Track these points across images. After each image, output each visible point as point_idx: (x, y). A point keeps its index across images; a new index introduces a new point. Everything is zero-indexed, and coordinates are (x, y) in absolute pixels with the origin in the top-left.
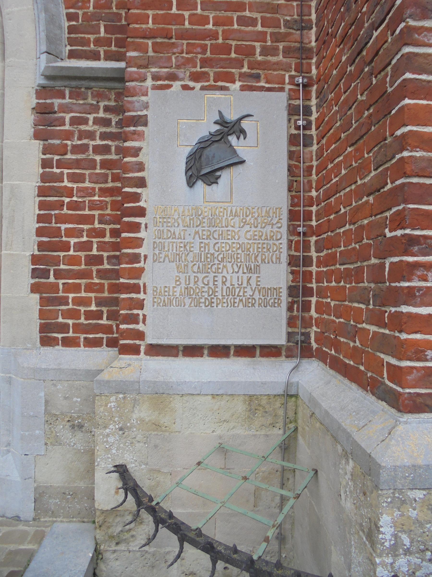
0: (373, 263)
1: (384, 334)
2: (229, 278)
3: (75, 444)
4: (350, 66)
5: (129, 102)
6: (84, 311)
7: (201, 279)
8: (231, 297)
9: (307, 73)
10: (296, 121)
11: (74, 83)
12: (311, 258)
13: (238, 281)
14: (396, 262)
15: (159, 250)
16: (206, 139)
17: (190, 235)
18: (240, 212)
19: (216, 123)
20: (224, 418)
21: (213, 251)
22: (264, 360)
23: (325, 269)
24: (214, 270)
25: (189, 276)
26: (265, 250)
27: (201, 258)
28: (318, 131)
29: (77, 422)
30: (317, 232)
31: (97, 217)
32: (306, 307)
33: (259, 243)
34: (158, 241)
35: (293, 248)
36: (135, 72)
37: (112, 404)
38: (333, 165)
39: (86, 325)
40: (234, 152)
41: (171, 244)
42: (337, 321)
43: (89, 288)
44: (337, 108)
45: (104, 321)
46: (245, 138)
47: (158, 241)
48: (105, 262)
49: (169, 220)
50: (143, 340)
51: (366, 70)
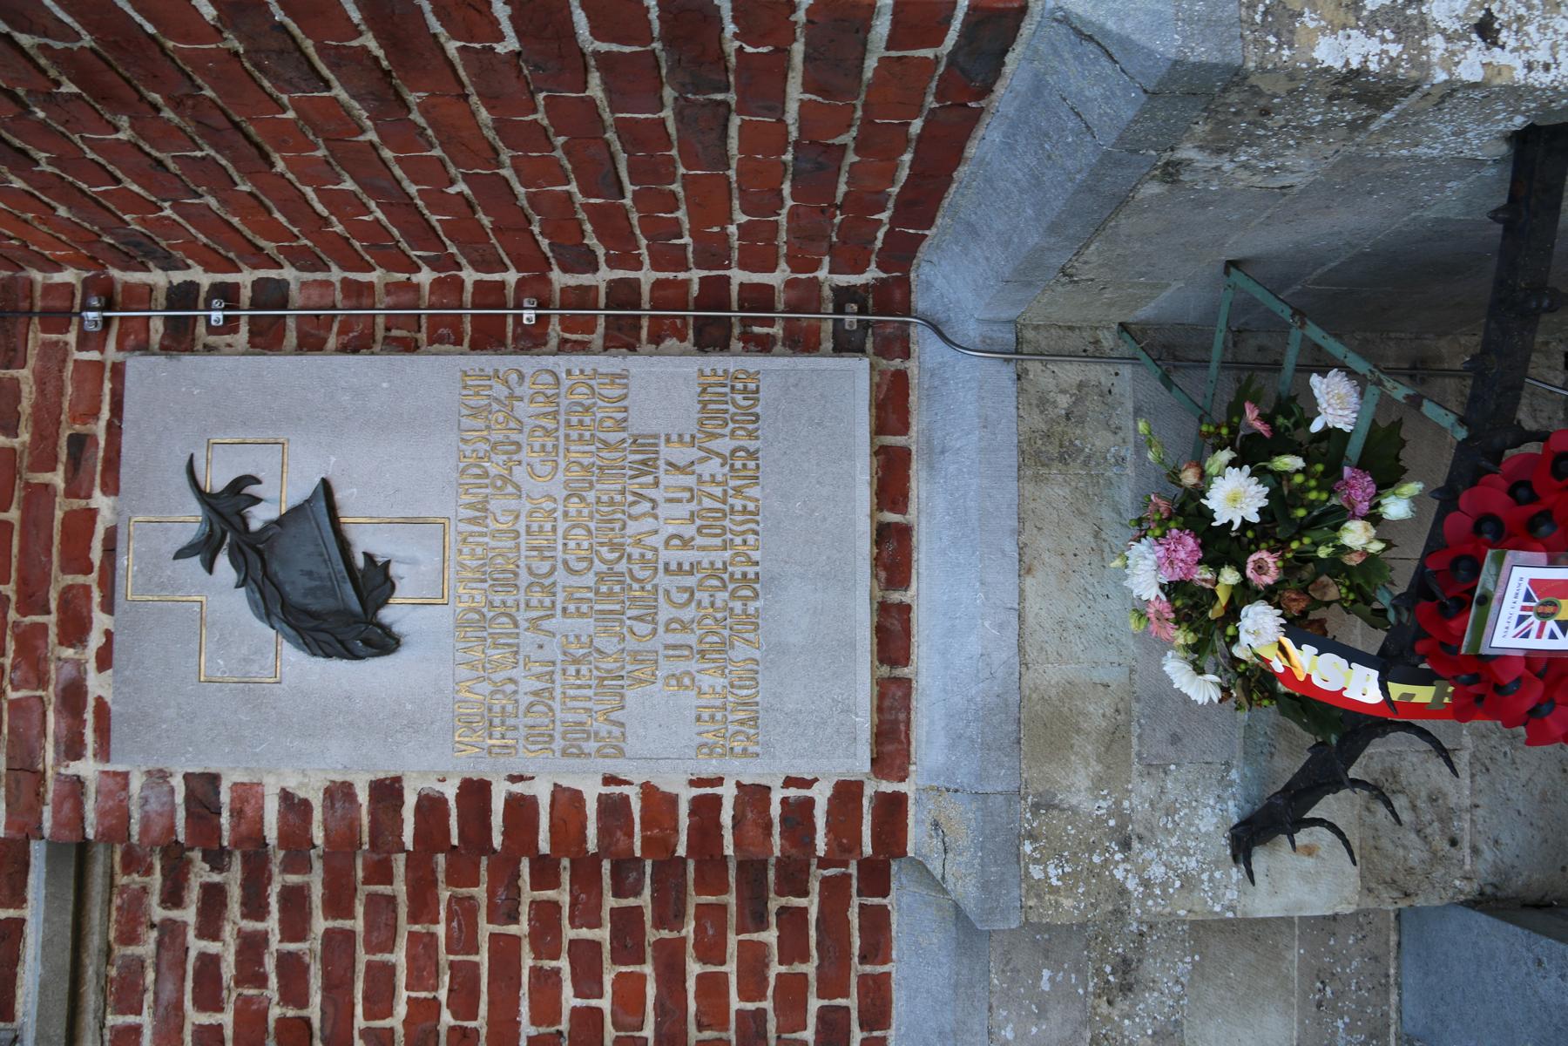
0: (604, 90)
1: (807, 58)
2: (671, 530)
3: (1177, 982)
4: (37, 163)
5: (145, 830)
6: (781, 963)
7: (675, 613)
8: (727, 523)
9: (73, 295)
10: (212, 330)
11: (91, 999)
12: (613, 285)
13: (679, 501)
14: (588, 17)
15: (589, 738)
16: (258, 596)
17: (541, 647)
18: (474, 495)
19: (209, 568)
20: (1089, 538)
21: (591, 575)
22: (917, 423)
23: (644, 242)
24: (648, 573)
25: (667, 647)
26: (587, 420)
27: (611, 612)
28: (241, 265)
29: (1111, 978)
30: (534, 266)
31: (497, 929)
32: (758, 298)
33: (567, 436)
34: (558, 744)
35: (586, 337)
36: (56, 812)
37: (1052, 871)
38: (333, 219)
39: (821, 958)
40: (297, 512)
41: (571, 704)
42: (789, 203)
43: (711, 951)
44: (167, 204)
45: (812, 904)
46: (258, 482)
47: (558, 744)
48: (631, 902)
49: (497, 709)
50: (859, 785)
51: (41, 115)
